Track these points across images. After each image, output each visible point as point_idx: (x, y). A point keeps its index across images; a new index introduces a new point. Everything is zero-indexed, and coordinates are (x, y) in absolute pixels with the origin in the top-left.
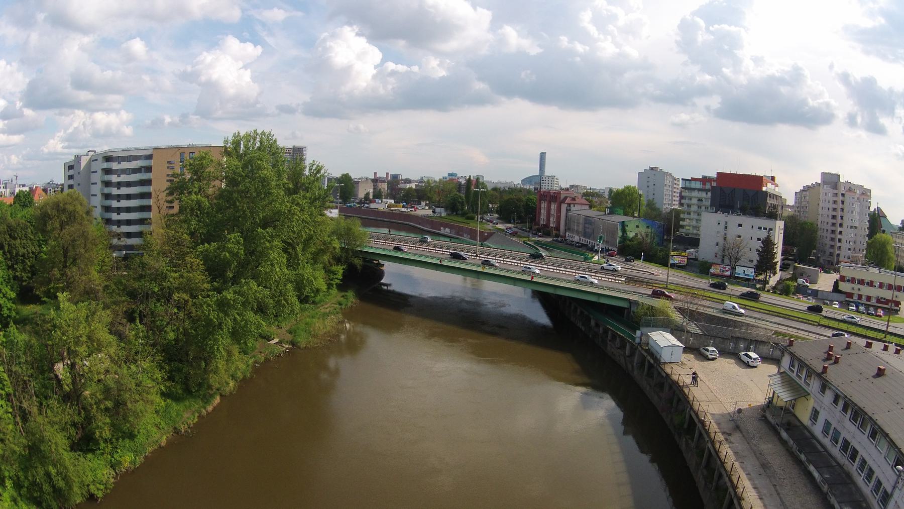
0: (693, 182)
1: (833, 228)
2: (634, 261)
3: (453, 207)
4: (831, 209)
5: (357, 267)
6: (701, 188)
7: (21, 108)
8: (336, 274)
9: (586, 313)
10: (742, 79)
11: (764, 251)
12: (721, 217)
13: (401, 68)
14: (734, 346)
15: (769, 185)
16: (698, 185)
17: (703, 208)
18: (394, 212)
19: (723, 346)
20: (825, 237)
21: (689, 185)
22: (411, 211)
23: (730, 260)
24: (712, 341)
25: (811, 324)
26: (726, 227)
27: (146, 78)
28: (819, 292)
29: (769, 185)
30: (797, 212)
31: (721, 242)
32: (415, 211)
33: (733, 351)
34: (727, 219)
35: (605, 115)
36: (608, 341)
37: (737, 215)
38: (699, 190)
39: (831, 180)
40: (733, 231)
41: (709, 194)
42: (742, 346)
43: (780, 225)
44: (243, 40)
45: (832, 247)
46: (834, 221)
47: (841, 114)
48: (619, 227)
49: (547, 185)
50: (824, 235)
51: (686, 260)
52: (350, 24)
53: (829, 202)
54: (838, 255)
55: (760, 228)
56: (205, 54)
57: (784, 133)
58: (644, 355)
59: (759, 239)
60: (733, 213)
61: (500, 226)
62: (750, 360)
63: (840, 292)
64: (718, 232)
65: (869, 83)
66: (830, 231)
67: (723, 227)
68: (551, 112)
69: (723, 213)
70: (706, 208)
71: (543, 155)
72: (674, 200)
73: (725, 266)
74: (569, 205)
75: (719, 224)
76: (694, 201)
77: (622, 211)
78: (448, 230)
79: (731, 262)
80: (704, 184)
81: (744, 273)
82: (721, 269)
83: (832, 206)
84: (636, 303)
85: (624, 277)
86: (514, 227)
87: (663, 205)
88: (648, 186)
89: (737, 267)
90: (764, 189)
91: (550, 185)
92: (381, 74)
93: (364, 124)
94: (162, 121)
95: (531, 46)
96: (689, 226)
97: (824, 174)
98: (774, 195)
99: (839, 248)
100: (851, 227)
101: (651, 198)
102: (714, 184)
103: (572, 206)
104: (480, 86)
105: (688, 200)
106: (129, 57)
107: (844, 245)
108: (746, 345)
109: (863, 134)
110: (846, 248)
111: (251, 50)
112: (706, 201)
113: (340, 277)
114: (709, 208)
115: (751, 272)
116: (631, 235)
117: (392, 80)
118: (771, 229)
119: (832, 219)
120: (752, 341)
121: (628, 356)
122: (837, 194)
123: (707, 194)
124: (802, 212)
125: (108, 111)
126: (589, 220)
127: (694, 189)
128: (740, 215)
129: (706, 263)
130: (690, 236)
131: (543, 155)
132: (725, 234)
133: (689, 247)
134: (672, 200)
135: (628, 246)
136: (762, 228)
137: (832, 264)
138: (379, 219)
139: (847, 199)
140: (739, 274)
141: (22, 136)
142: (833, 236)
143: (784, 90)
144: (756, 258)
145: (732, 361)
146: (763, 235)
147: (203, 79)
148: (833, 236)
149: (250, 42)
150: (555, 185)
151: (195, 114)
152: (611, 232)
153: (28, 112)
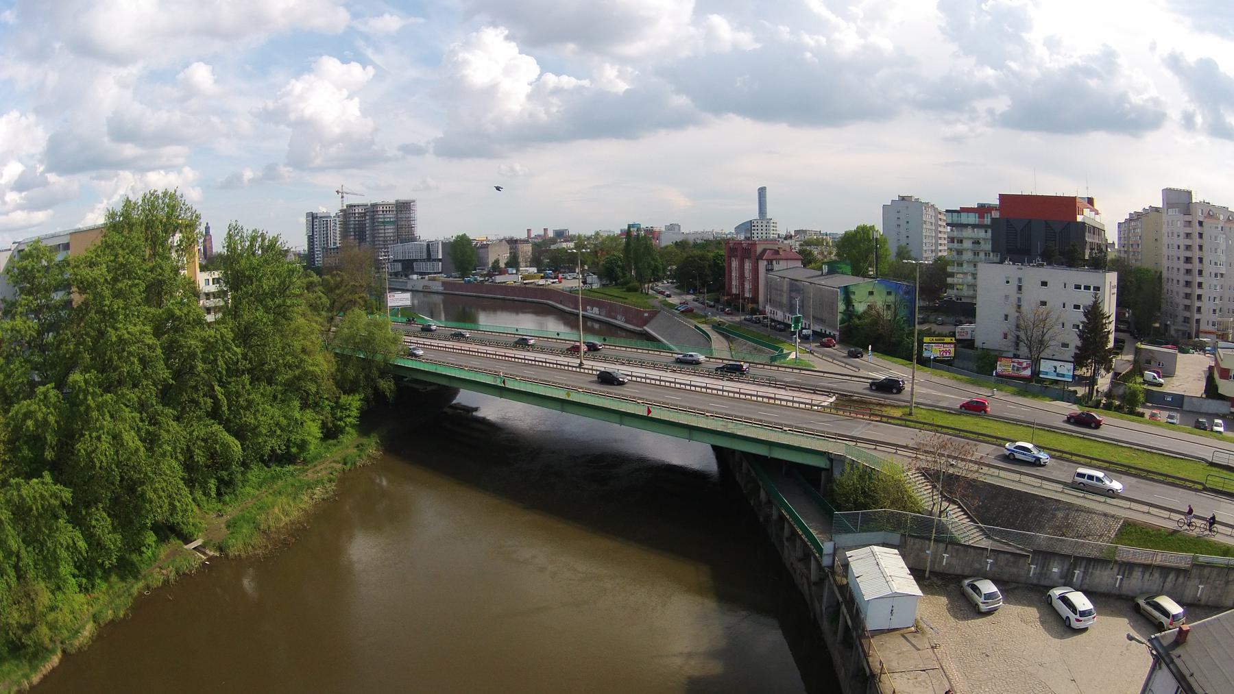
0: (964, 215)
1: (1188, 278)
2: (862, 356)
3: (610, 274)
4: (1182, 247)
5: (386, 396)
6: (977, 223)
7: (42, 173)
8: (346, 409)
9: (753, 474)
10: (1035, 73)
11: (1091, 331)
12: (1009, 270)
13: (567, 81)
14: (1038, 571)
15: (1086, 212)
16: (972, 219)
17: (982, 255)
18: (527, 286)
19: (1015, 570)
20: (1175, 294)
21: (957, 219)
22: (553, 283)
23: (1029, 347)
24: (990, 561)
25: (1190, 488)
26: (1020, 288)
27: (215, 120)
28: (1186, 400)
29: (1086, 212)
30: (1122, 253)
31: (1013, 314)
32: (560, 282)
33: (1035, 581)
34: (1020, 274)
35: (853, 132)
36: (784, 540)
37: (1038, 266)
38: (974, 226)
39: (1179, 201)
40: (1032, 294)
41: (990, 231)
42: (1055, 570)
43: (1112, 278)
44: (345, 61)
45: (1187, 308)
46: (1189, 266)
47: (1174, 114)
48: (840, 296)
49: (760, 232)
50: (1174, 290)
51: (952, 350)
52: (495, 25)
53: (1179, 236)
54: (1198, 321)
55: (1078, 287)
56: (293, 81)
57: (1098, 143)
58: (838, 600)
59: (1077, 307)
60: (1030, 262)
61: (674, 300)
62: (1072, 617)
63: (1222, 398)
64: (1007, 297)
65: (1208, 67)
66: (1182, 283)
67: (1016, 288)
68: (780, 132)
69: (1014, 264)
70: (986, 254)
71: (762, 192)
72: (941, 244)
73: (1021, 360)
74: (770, 262)
75: (1008, 282)
76: (967, 244)
77: (848, 269)
78: (596, 310)
79: (1030, 351)
80: (982, 217)
81: (1055, 371)
82: (1014, 366)
83: (1183, 242)
84: (841, 459)
85: (834, 394)
86: (694, 300)
87: (922, 254)
88: (899, 225)
89: (1042, 360)
90: (1079, 218)
91: (764, 232)
92: (538, 92)
93: (521, 163)
94: (239, 177)
95: (746, 40)
96: (962, 285)
97: (1168, 193)
98: (1094, 227)
99: (1199, 309)
100: (1216, 275)
101: (903, 243)
102: (996, 214)
103: (774, 262)
104: (681, 101)
105: (958, 242)
106: (190, 92)
107: (1206, 305)
108: (1066, 567)
109: (1203, 139)
110: (1209, 309)
111: (356, 72)
112: (985, 244)
113: (355, 413)
114: (991, 254)
115: (1067, 369)
116: (860, 308)
117: (555, 100)
118: (1096, 289)
119: (1185, 262)
120: (1077, 561)
121: (815, 584)
122: (1190, 222)
123: (986, 232)
124: (1132, 253)
125: (168, 168)
126: (796, 285)
127: (965, 226)
128: (1042, 265)
129: (987, 352)
130: (963, 300)
131: (762, 192)
132: (1019, 299)
133: (962, 318)
134: (937, 244)
135: (856, 327)
136: (1082, 287)
137: (1190, 337)
138: (516, 298)
139: (1206, 229)
140: (1046, 373)
141: (50, 212)
142: (1188, 290)
143: (1093, 83)
144: (1075, 341)
145: (1032, 613)
146: (1086, 299)
147: (293, 116)
148: (1188, 290)
149: (354, 61)
150: (772, 232)
151: (288, 164)
152: (826, 303)
153: (52, 178)
